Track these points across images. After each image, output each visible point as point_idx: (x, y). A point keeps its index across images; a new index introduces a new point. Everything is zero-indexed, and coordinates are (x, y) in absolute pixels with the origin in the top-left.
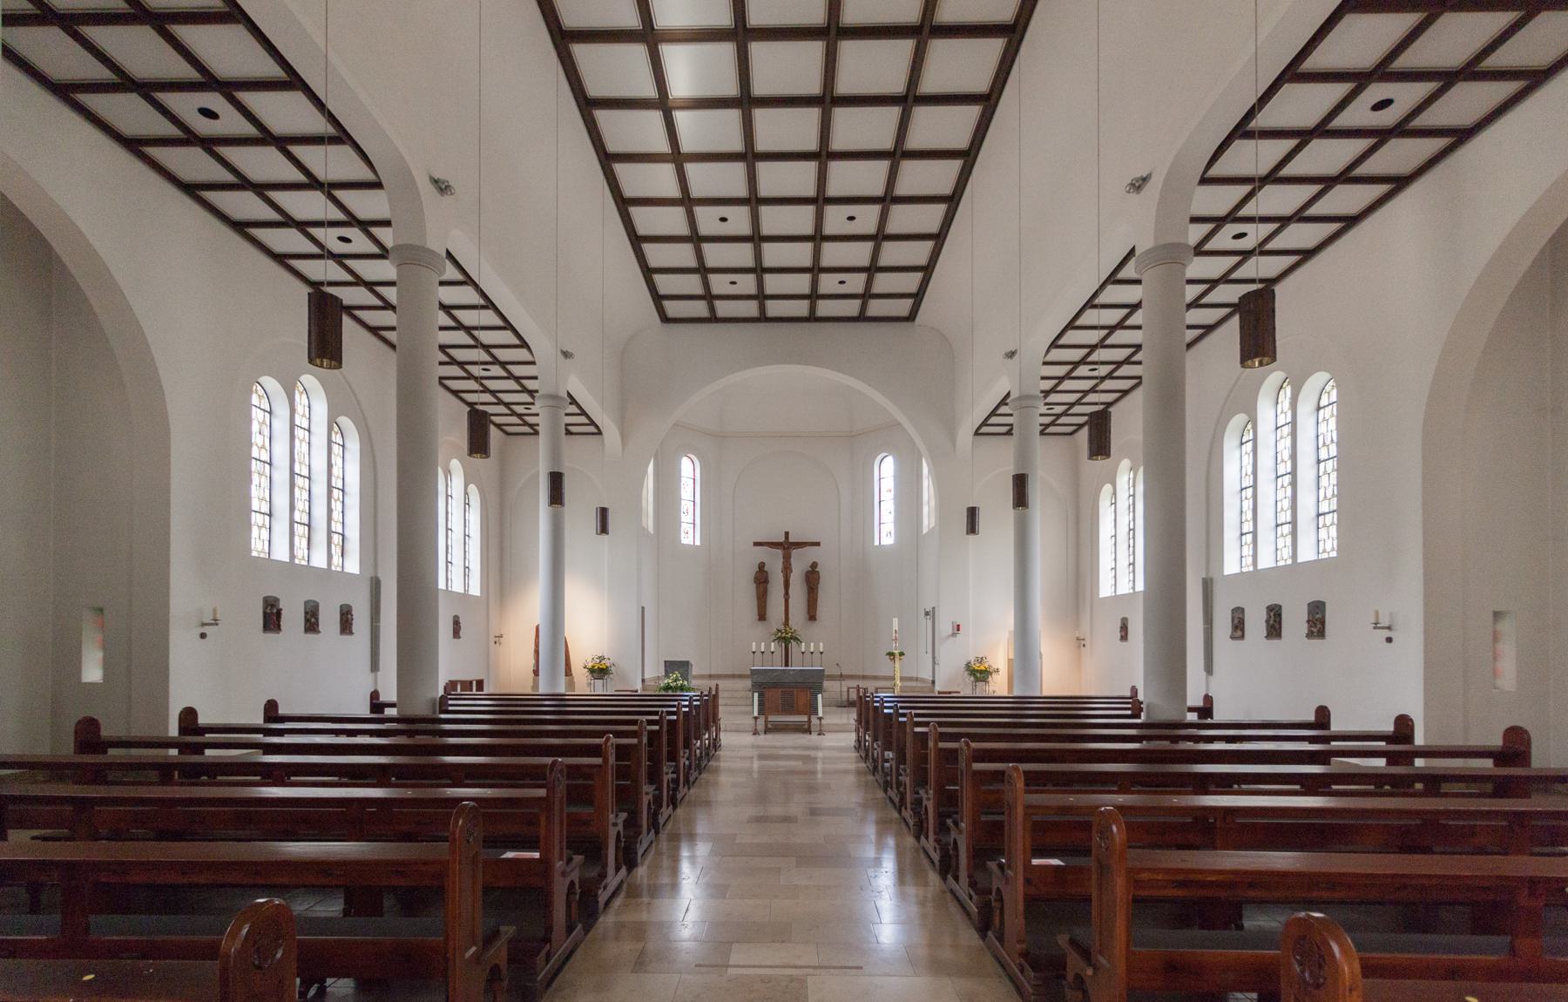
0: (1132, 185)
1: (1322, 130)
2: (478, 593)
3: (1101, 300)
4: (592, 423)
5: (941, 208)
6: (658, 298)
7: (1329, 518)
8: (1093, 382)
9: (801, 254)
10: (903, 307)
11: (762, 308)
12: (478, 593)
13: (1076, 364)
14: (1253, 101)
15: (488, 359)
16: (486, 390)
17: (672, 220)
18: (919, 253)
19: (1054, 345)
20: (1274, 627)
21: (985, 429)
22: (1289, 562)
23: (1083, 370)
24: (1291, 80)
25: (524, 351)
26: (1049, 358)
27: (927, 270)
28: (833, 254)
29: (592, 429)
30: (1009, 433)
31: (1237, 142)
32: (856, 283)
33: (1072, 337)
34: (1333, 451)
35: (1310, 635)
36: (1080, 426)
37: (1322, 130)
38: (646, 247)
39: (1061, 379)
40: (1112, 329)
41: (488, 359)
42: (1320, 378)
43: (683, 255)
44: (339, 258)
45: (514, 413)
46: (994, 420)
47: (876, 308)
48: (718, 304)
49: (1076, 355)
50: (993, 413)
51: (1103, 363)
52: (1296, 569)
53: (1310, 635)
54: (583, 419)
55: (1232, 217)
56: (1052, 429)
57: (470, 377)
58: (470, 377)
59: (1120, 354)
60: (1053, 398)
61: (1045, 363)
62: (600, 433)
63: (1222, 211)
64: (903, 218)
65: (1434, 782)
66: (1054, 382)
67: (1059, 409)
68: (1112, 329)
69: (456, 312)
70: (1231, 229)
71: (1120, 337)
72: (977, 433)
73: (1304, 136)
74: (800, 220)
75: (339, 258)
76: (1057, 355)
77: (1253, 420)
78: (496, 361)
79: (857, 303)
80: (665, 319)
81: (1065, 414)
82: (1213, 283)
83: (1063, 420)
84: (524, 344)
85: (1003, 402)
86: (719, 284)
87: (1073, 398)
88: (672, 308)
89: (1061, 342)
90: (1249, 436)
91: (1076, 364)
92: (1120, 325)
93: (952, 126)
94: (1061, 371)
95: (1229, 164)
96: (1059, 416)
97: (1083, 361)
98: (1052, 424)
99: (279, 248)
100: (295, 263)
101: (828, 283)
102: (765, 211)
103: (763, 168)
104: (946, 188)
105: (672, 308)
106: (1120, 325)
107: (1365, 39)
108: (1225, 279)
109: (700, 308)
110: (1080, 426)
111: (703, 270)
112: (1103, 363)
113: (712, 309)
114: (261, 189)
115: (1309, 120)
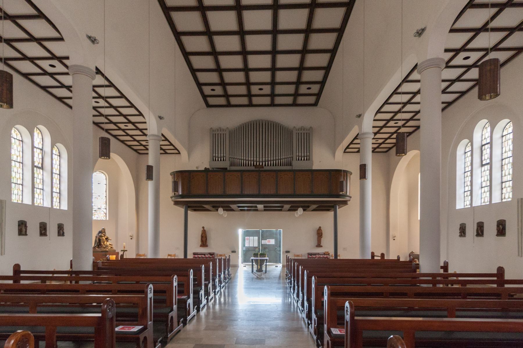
0: (418, 33)
1: (485, 28)
2: (66, 208)
3: (383, 110)
4: (176, 149)
5: (334, 35)
6: (205, 97)
7: (507, 184)
8: (377, 145)
9: (266, 77)
10: (312, 100)
11: (250, 101)
12: (66, 208)
13: (388, 121)
14: (401, 81)
15: (126, 121)
16: (128, 135)
17: (208, 62)
18: (318, 75)
19: (379, 112)
20: (480, 231)
21: (348, 150)
22: (488, 203)
23: (392, 123)
24: (470, 8)
25: (141, 117)
26: (377, 118)
27: (327, 69)
28: (281, 76)
29: (176, 151)
30: (358, 152)
31: (468, 10)
32: (291, 89)
33: (387, 108)
34: (510, 154)
35: (461, 236)
36: (390, 148)
37: (485, 28)
38: (184, 39)
39: (381, 128)
40: (405, 104)
41: (126, 121)
42: (504, 122)
43: (214, 77)
44: (52, 75)
45: (141, 145)
46: (352, 146)
47: (301, 100)
48: (221, 58)
49: (388, 116)
50: (351, 143)
51: (400, 120)
52: (473, 209)
53: (461, 236)
54: (171, 147)
55: (464, 49)
56: (377, 150)
57: (120, 129)
58: (120, 129)
59: (408, 116)
60: (378, 136)
61: (374, 120)
62: (179, 153)
63: (458, 46)
64: (312, 60)
65: (453, 283)
66: (384, 122)
67: (380, 141)
68: (405, 104)
69: (119, 109)
70: (463, 55)
71: (409, 108)
72: (344, 152)
73: (477, 31)
74: (265, 61)
75: (52, 75)
76: (380, 116)
77: (471, 141)
78: (130, 122)
79: (298, 57)
80: (208, 106)
81: (383, 143)
82: (453, 82)
83: (383, 146)
84: (141, 114)
85: (356, 138)
86: (231, 90)
87: (386, 136)
88: (212, 101)
89: (382, 110)
90: (469, 149)
91: (388, 121)
92: (409, 102)
93: (324, 41)
94: (381, 123)
95: (465, 22)
96: (381, 144)
97: (392, 119)
98: (378, 147)
99: (59, 95)
100: (50, 90)
101: (279, 89)
102: (250, 58)
103: (248, 38)
104: (330, 46)
105: (212, 101)
106: (409, 102)
107: (476, 18)
108: (458, 79)
109: (222, 101)
110: (390, 148)
111: (219, 70)
112: (400, 120)
113: (228, 101)
114: (32, 60)
115: (479, 24)
